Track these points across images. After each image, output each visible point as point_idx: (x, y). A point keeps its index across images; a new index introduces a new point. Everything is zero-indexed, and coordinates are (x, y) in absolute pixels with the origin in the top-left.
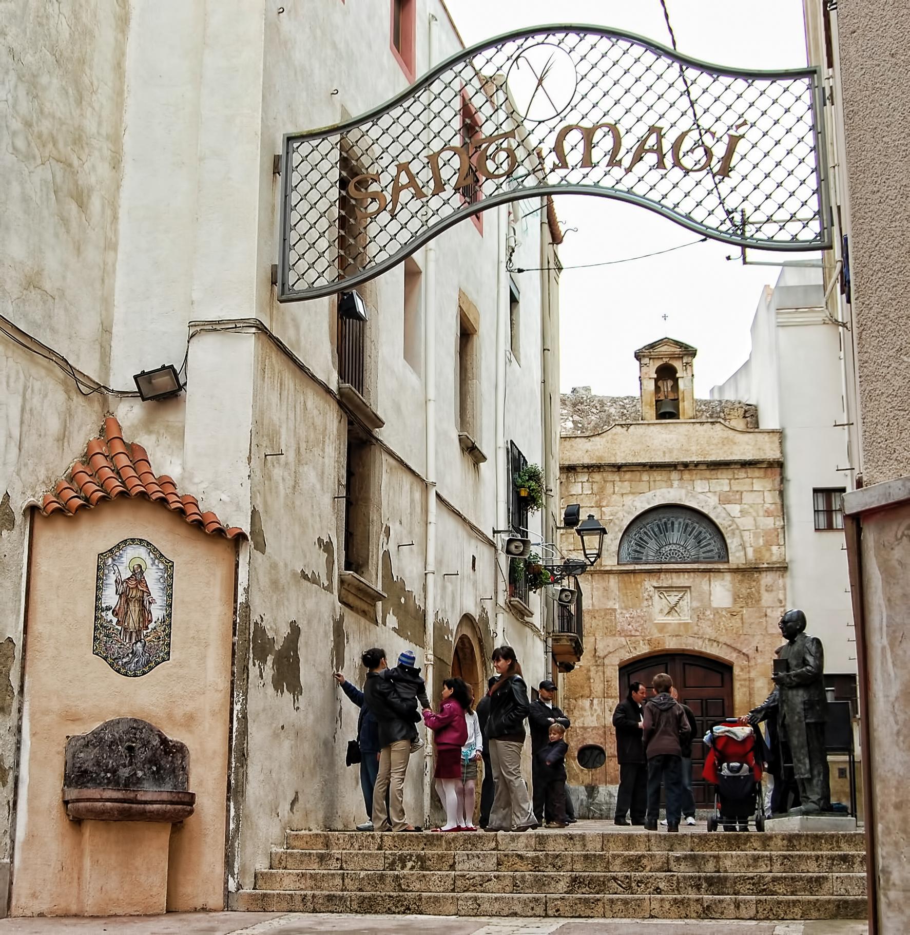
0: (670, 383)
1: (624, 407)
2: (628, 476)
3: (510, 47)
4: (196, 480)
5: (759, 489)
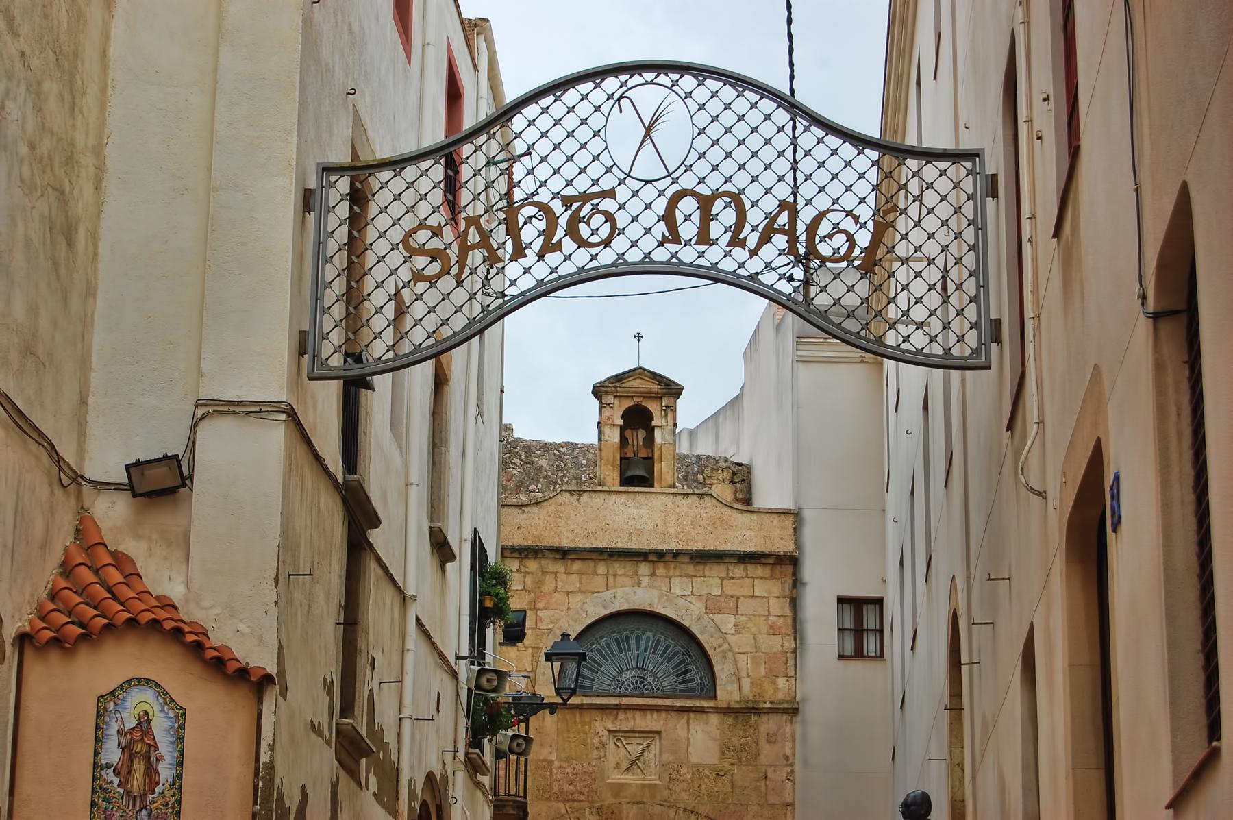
0: (642, 434)
1: (560, 458)
2: (577, 566)
3: (611, 84)
4: (205, 604)
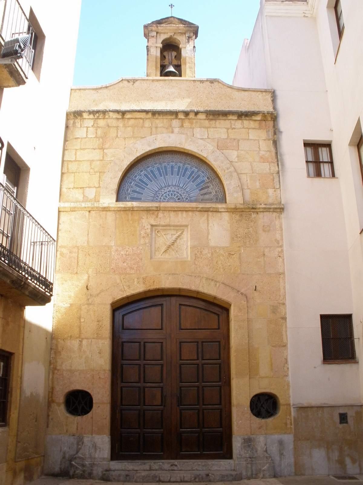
5: (254, 136)
